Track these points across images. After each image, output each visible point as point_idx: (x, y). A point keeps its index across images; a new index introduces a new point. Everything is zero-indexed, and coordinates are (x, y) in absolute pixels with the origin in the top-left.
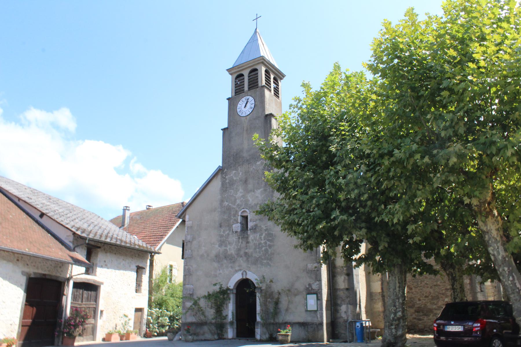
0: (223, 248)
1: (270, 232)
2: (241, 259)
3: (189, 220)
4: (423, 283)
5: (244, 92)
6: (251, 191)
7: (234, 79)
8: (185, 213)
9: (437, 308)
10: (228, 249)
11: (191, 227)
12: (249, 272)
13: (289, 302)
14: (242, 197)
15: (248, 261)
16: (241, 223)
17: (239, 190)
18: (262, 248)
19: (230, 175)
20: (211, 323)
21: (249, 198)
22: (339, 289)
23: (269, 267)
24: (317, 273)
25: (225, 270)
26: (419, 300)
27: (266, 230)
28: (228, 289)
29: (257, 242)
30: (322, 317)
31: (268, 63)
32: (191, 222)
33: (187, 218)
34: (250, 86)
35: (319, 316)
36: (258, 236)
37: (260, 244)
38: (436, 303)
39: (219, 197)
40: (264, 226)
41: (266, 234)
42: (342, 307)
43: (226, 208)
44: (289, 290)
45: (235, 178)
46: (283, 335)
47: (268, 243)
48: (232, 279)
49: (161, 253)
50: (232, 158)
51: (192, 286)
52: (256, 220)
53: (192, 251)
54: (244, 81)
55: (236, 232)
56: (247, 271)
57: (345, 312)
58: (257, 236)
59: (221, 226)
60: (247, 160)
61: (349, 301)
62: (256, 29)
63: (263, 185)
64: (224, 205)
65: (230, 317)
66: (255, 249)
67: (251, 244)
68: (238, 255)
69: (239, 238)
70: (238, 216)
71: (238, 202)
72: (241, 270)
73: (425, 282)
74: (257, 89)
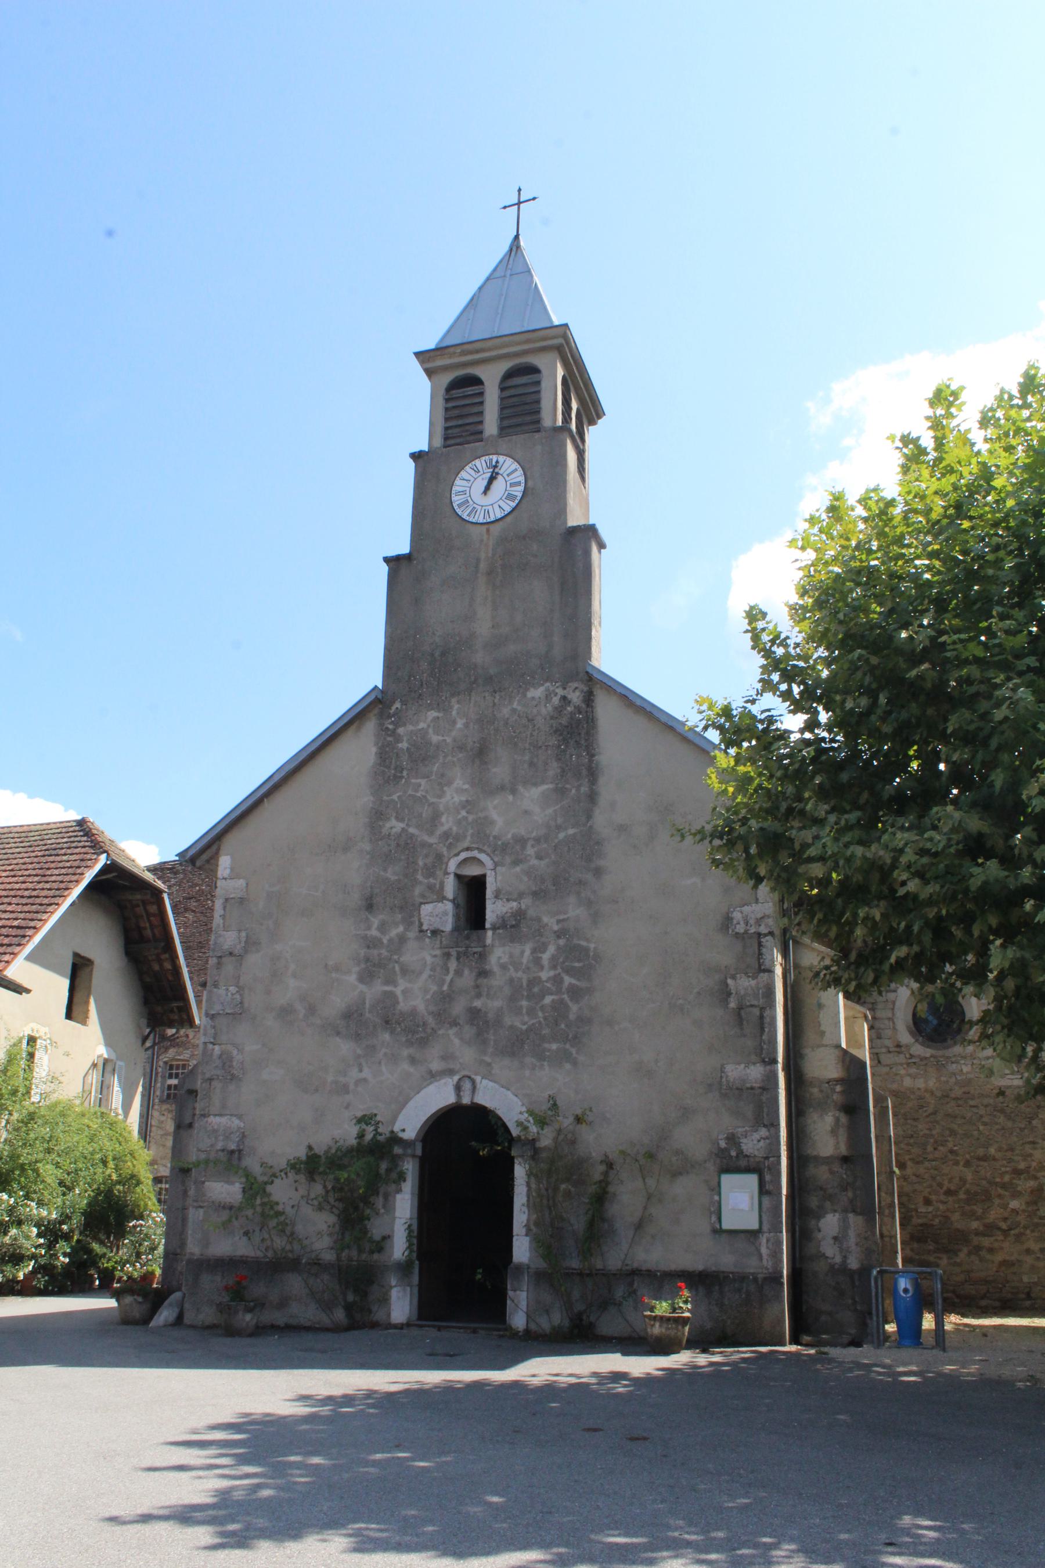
0: (379, 988)
1: (575, 941)
2: (452, 1032)
3: (234, 875)
4: (941, 1148)
5: (538, 431)
6: (502, 788)
7: (442, 392)
8: (214, 848)
9: (981, 1228)
10: (398, 991)
11: (242, 901)
12: (485, 1082)
13: (649, 1197)
14: (464, 807)
15: (485, 1042)
16: (453, 901)
17: (450, 783)
18: (543, 997)
19: (417, 723)
21: (494, 815)
22: (816, 1158)
24: (764, 1098)
25: (384, 1069)
26: (927, 1202)
27: (559, 935)
28: (394, 1139)
29: (520, 974)
30: (776, 1254)
31: (572, 356)
32: (241, 883)
35: (764, 1251)
36: (527, 953)
37: (533, 982)
38: (980, 1211)
39: (367, 800)
41: (559, 948)
42: (823, 1221)
44: (650, 1156)
45: (435, 739)
46: (661, 1319)
47: (568, 980)
48: (411, 1104)
49: (28, 991)
50: (425, 665)
51: (236, 1122)
52: (521, 896)
53: (241, 989)
54: (482, 403)
55: (435, 932)
56: (478, 1079)
57: (835, 1238)
58: (523, 952)
59: (370, 906)
60: (489, 680)
61: (851, 1201)
62: (517, 237)
63: (551, 773)
64: (385, 831)
65: (399, 1248)
66: (513, 999)
67: (498, 980)
68: (443, 1016)
69: (448, 955)
70: (446, 873)
71: (447, 823)
72: (451, 1072)
73: (950, 1145)
74: (537, 436)
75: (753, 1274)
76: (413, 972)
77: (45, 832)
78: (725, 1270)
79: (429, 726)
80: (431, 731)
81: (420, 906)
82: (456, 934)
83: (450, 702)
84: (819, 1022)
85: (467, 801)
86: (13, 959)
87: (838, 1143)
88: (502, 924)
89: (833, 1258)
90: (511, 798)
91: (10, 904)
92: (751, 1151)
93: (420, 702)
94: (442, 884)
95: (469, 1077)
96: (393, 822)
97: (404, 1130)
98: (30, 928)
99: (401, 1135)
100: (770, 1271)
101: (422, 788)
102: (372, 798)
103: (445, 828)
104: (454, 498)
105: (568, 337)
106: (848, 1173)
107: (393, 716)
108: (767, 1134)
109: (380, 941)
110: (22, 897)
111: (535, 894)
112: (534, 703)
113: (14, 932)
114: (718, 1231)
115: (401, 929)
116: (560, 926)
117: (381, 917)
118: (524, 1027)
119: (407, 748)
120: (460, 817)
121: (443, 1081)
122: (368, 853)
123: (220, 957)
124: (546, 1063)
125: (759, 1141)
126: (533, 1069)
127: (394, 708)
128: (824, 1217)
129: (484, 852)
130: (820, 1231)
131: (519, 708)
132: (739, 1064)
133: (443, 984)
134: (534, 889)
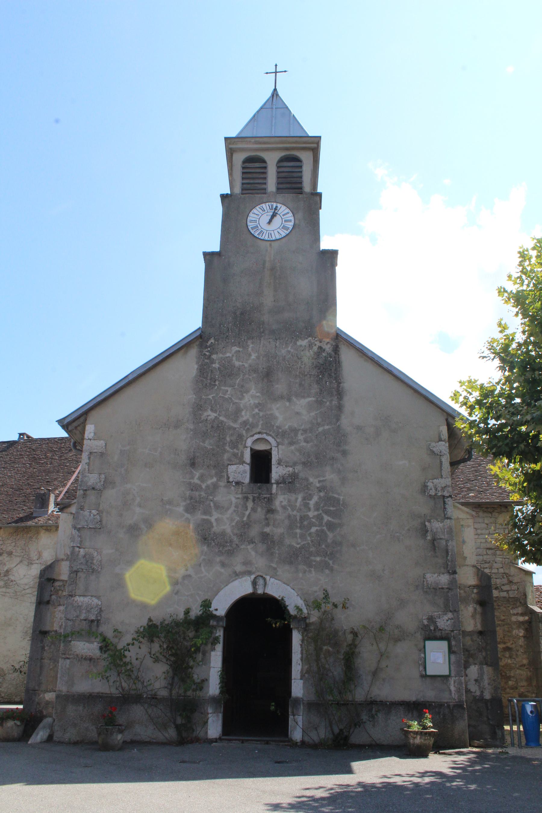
1: (331, 494)
3: (97, 437)
6: (282, 397)
10: (213, 519)
14: (257, 407)
15: (272, 554)
17: (247, 392)
19: (225, 353)
20: (154, 697)
23: (327, 571)
24: (449, 594)
25: (203, 569)
27: (320, 490)
32: (102, 443)
33: (90, 429)
36: (300, 499)
39: (191, 397)
40: (316, 480)
41: (320, 498)
43: (209, 426)
45: (237, 364)
47: (326, 518)
48: (222, 593)
53: (100, 512)
55: (238, 483)
56: (268, 578)
57: (476, 680)
59: (193, 464)
60: (273, 332)
63: (313, 391)
64: (203, 417)
66: (291, 527)
67: (280, 516)
71: (245, 416)
72: (249, 573)
74: (301, 196)
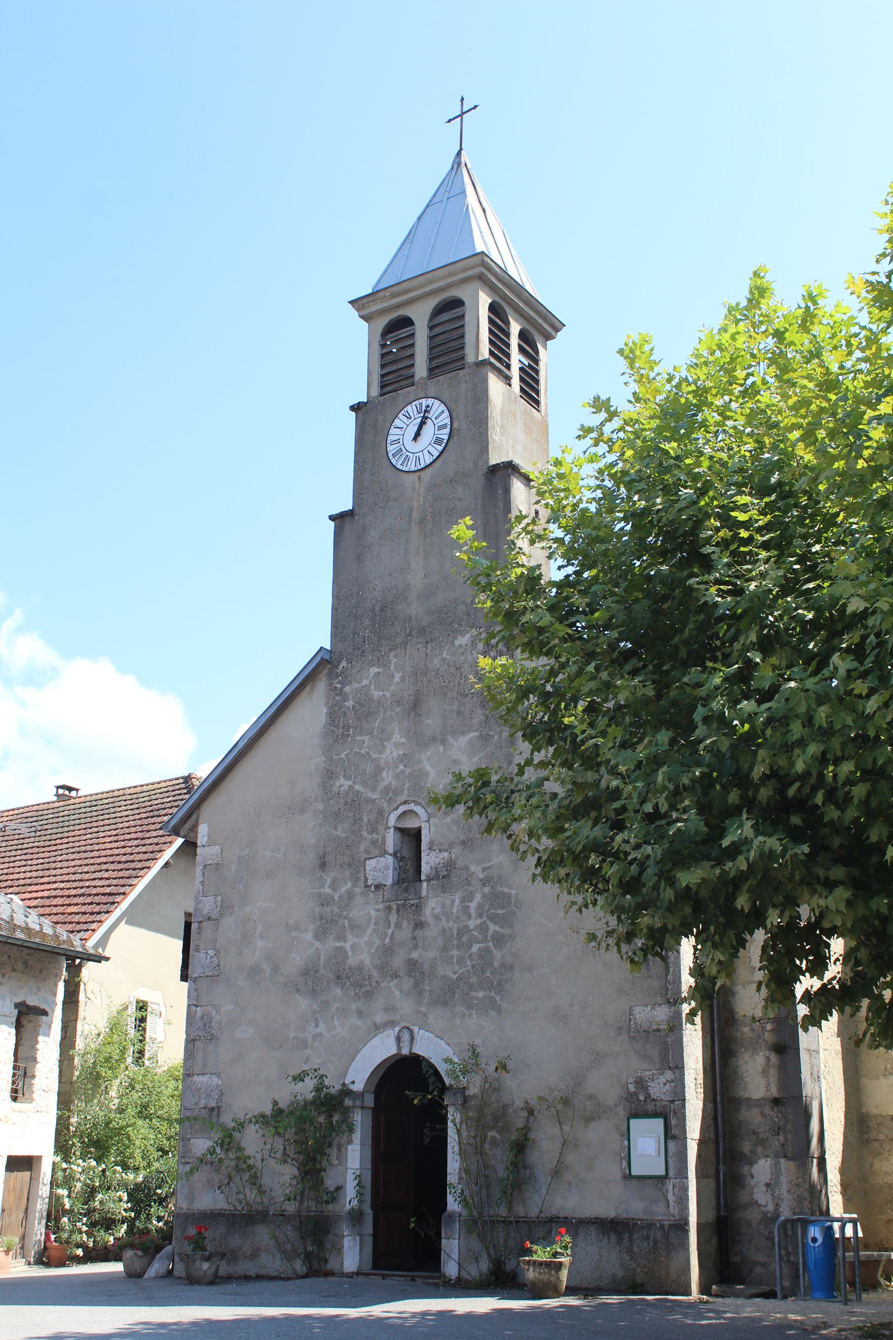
0: (332, 943)
1: (499, 889)
6: (434, 739)
10: (348, 946)
12: (422, 1032)
14: (401, 761)
15: (420, 993)
16: (395, 855)
17: (389, 738)
22: (748, 1100)
25: (336, 1023)
27: (484, 882)
28: (346, 1092)
31: (500, 280)
34: (435, 363)
35: (671, 1197)
36: (457, 902)
39: (319, 760)
41: (484, 896)
42: (755, 1166)
44: (566, 1102)
45: (376, 694)
47: (493, 928)
50: (367, 622)
52: (451, 846)
53: (217, 952)
55: (378, 887)
56: (416, 1029)
57: (768, 1185)
58: (453, 902)
59: (323, 865)
60: (422, 631)
63: (476, 721)
64: (335, 789)
66: (445, 948)
67: (432, 931)
69: (389, 908)
71: (388, 778)
72: (391, 1024)
74: (461, 373)
75: (659, 1221)
76: (360, 927)
77: (154, 792)
78: (635, 1217)
79: (370, 683)
80: (372, 687)
81: (365, 862)
82: (396, 887)
83: (388, 657)
84: (749, 957)
85: (404, 755)
86: (99, 927)
87: (769, 1085)
88: (435, 876)
89: (766, 1206)
90: (441, 748)
91: (107, 870)
92: (658, 1095)
93: (363, 659)
94: (384, 838)
95: (408, 1028)
96: (342, 781)
97: (353, 1082)
98: (119, 894)
99: (351, 1087)
100: (677, 1217)
101: (366, 745)
102: (324, 759)
103: (386, 783)
104: (390, 448)
105: (487, 263)
106: (780, 1116)
107: (340, 675)
108: (673, 1077)
109: (332, 897)
110: (119, 862)
111: (463, 843)
112: (461, 651)
113: (104, 899)
114: (628, 1177)
115: (349, 885)
116: (485, 873)
117: (333, 874)
118: (455, 977)
119: (353, 706)
120: (398, 771)
121: (386, 1033)
122: (321, 813)
123: (201, 922)
124: (474, 1012)
125: (665, 1084)
126: (463, 1018)
127: (340, 667)
128: (756, 1163)
129: (419, 804)
130: (752, 1177)
131: (448, 657)
132: (646, 1006)
133: (385, 938)
134: (462, 838)
